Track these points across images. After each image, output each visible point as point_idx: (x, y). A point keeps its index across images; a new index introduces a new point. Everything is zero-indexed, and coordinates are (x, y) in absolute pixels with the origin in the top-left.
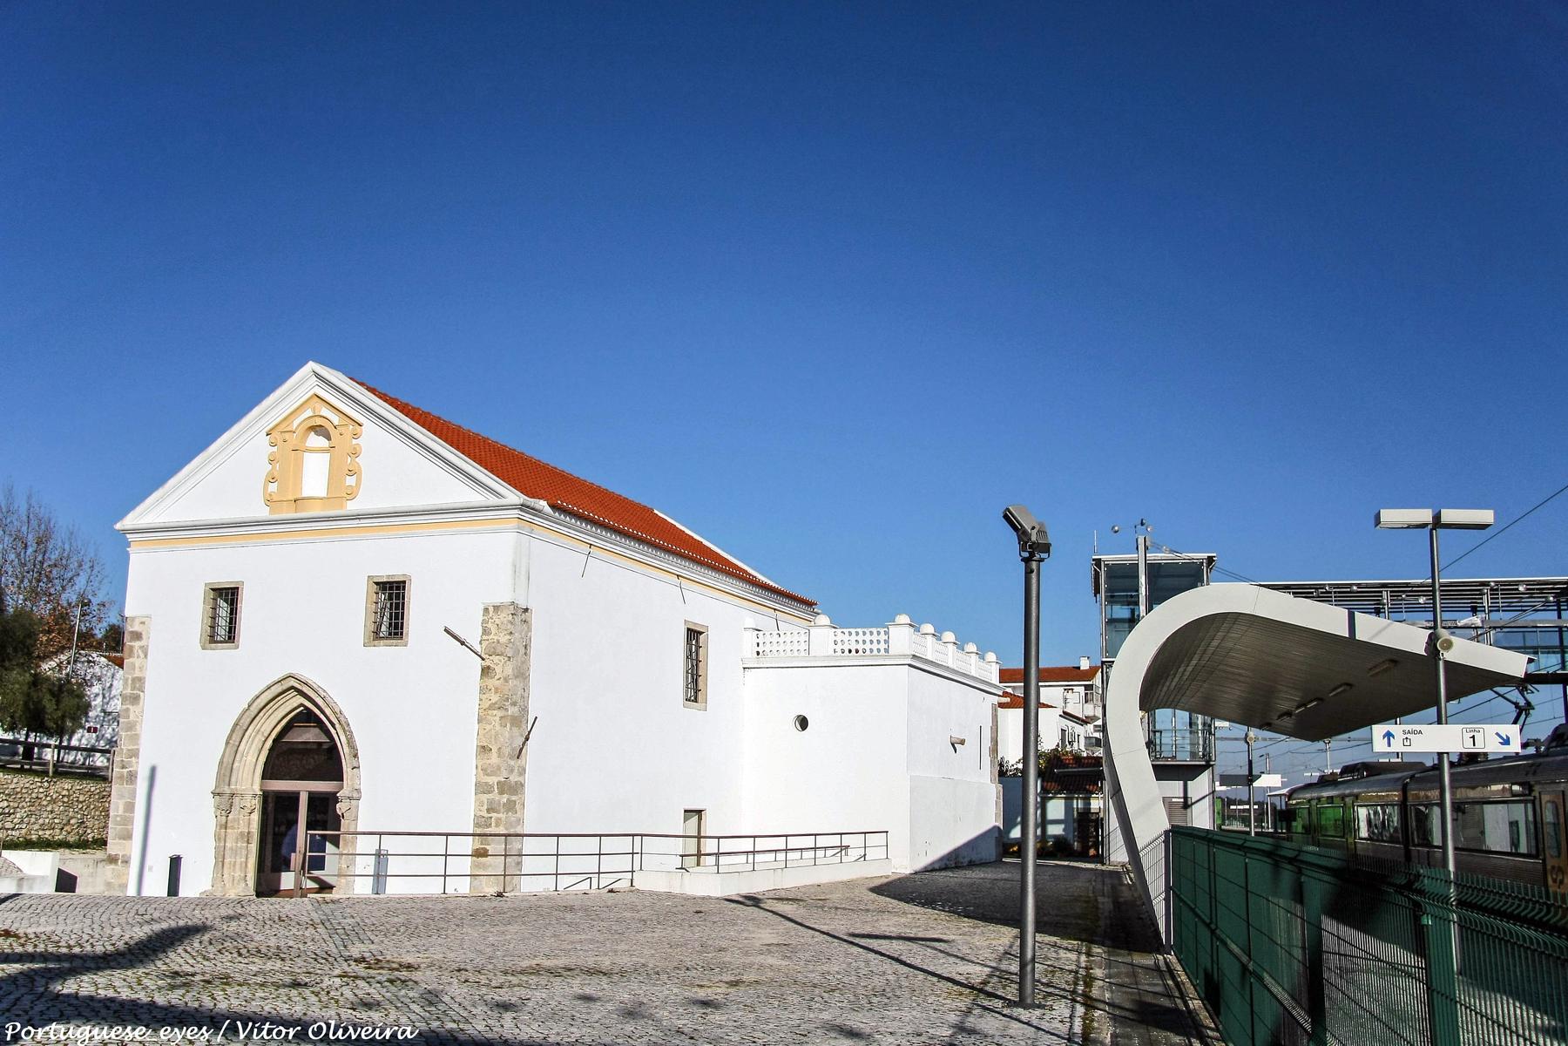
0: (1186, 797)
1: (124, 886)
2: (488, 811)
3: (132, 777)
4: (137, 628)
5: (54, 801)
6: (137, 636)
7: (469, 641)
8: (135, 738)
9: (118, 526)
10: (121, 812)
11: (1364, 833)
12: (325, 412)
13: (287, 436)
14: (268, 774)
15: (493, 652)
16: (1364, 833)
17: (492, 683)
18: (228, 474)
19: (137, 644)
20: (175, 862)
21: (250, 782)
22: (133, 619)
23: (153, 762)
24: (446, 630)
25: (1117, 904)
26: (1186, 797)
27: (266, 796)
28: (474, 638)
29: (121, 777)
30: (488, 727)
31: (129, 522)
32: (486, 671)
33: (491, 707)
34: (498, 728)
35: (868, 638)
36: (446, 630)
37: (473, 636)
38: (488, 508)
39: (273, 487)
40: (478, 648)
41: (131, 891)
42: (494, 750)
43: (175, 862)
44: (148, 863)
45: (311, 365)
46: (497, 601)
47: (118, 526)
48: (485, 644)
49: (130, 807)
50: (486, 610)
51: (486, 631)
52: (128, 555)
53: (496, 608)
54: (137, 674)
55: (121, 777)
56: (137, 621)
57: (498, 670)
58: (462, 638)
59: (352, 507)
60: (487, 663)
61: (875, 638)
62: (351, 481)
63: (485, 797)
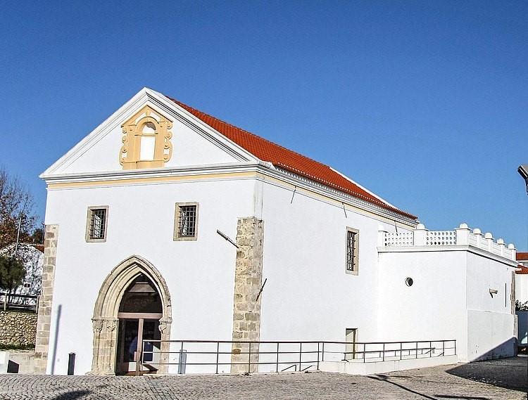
1: (45, 370)
2: (240, 329)
3: (49, 311)
6: (52, 235)
8: (50, 290)
9: (41, 176)
12: (153, 115)
17: (242, 260)
18: (100, 148)
19: (51, 239)
20: (72, 357)
21: (112, 313)
27: (121, 321)
32: (239, 254)
34: (246, 284)
38: (240, 167)
39: (125, 155)
41: (48, 372)
43: (72, 357)
45: (145, 90)
47: (41, 176)
49: (48, 327)
54: (51, 256)
58: (227, 235)
59: (168, 166)
62: (166, 152)
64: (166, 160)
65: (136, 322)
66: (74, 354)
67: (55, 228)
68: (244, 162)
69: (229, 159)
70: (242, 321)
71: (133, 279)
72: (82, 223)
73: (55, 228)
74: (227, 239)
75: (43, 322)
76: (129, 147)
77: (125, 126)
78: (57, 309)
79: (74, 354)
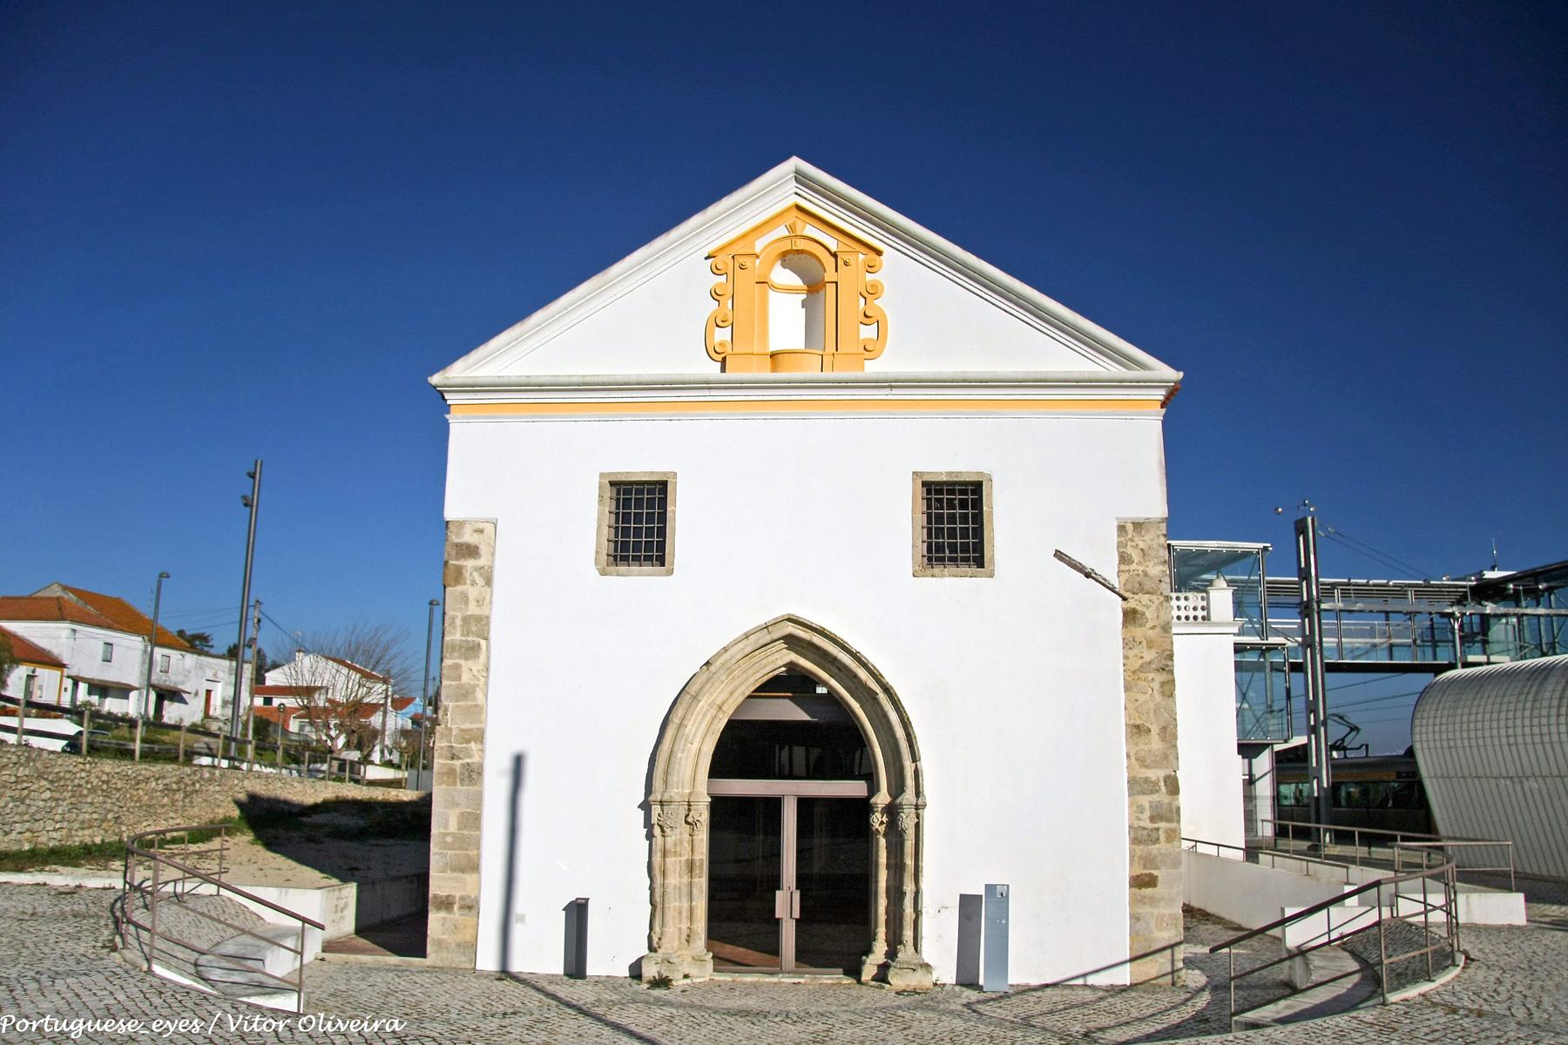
0: (1250, 774)
1: (471, 948)
2: (1152, 819)
3: (473, 774)
4: (468, 537)
5: (93, 790)
6: (471, 551)
7: (1100, 570)
8: (477, 712)
9: (435, 379)
10: (453, 827)
12: (811, 230)
13: (747, 261)
14: (719, 769)
17: (1138, 632)
18: (645, 307)
19: (469, 564)
20: (577, 913)
21: (693, 781)
22: (461, 524)
23: (517, 748)
24: (1059, 555)
25: (238, 803)
26: (1250, 774)
27: (719, 806)
29: (451, 772)
30: (1142, 698)
31: (460, 371)
32: (1130, 616)
34: (1158, 698)
35: (1182, 603)
36: (1059, 555)
37: (1108, 568)
38: (1120, 384)
39: (722, 335)
41: (487, 961)
42: (1155, 730)
43: (577, 913)
44: (519, 906)
45: (795, 162)
46: (1140, 514)
47: (435, 379)
48: (1125, 576)
49: (473, 820)
50: (1122, 529)
51: (1124, 559)
52: (446, 425)
53: (1138, 526)
54: (473, 609)
55: (451, 772)
56: (468, 530)
58: (1089, 565)
59: (872, 368)
60: (1132, 604)
61: (1191, 604)
62: (868, 332)
63: (1145, 800)
64: (869, 351)
65: (773, 805)
66: (998, 896)
67: (481, 531)
68: (1138, 374)
69: (1063, 359)
70: (1155, 797)
71: (877, 689)
72: (587, 521)
73: (481, 531)
74: (1088, 575)
75: (454, 804)
76: (734, 304)
77: (719, 261)
78: (507, 764)
79: (998, 896)
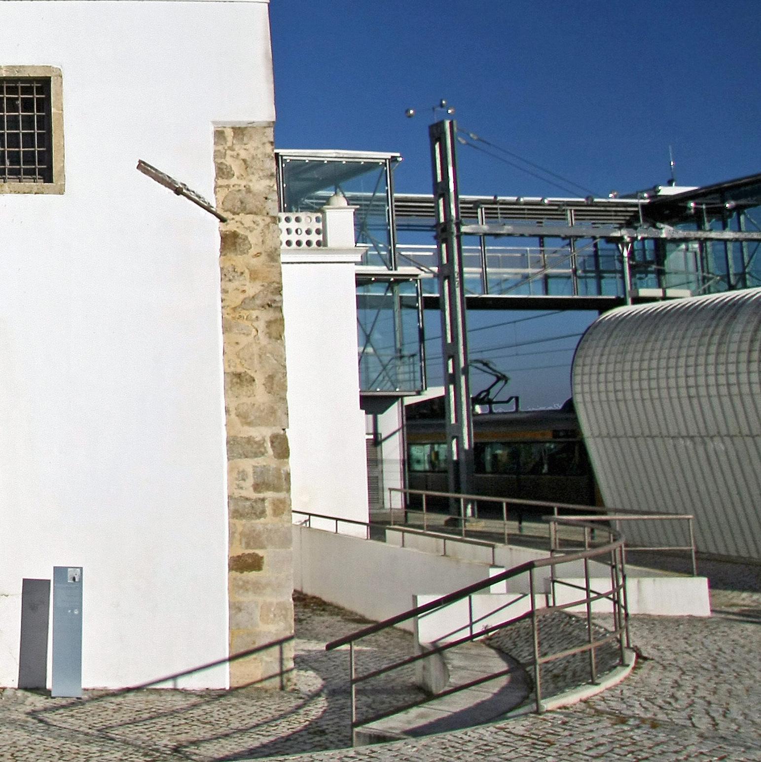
2: (257, 487)
11: (670, 147)
15: (241, 206)
16: (670, 147)
17: (239, 260)
24: (143, 167)
27: (508, 519)
28: (204, 183)
30: (244, 340)
32: (230, 241)
33: (245, 304)
35: (293, 225)
36: (143, 167)
37: (204, 183)
40: (211, 199)
42: (260, 379)
46: (242, 118)
48: (223, 193)
50: (219, 135)
51: (222, 171)
53: (239, 131)
57: (253, 238)
58: (179, 178)
60: (231, 226)
61: (304, 226)
63: (248, 465)
